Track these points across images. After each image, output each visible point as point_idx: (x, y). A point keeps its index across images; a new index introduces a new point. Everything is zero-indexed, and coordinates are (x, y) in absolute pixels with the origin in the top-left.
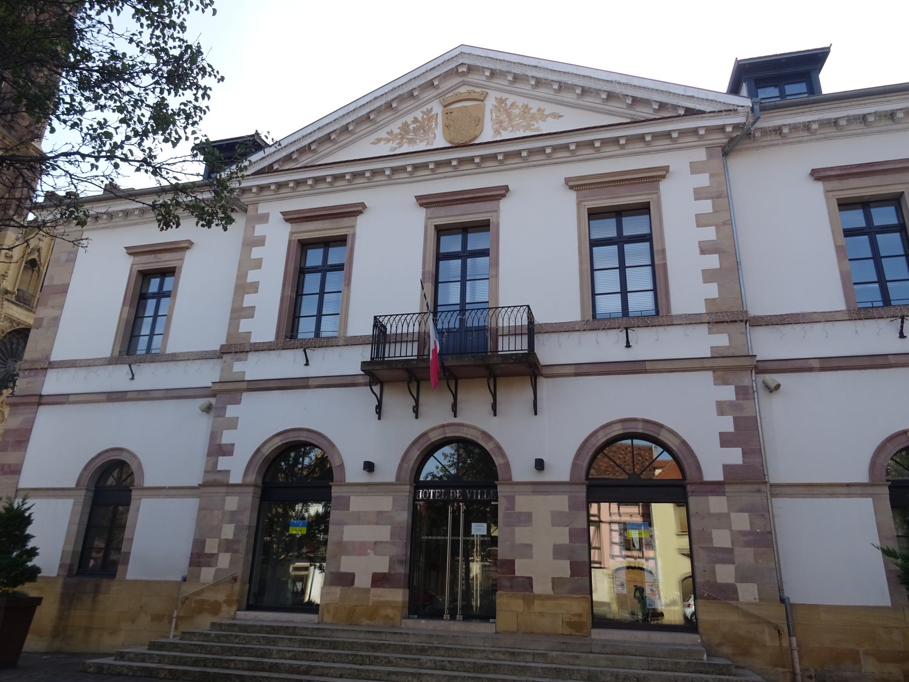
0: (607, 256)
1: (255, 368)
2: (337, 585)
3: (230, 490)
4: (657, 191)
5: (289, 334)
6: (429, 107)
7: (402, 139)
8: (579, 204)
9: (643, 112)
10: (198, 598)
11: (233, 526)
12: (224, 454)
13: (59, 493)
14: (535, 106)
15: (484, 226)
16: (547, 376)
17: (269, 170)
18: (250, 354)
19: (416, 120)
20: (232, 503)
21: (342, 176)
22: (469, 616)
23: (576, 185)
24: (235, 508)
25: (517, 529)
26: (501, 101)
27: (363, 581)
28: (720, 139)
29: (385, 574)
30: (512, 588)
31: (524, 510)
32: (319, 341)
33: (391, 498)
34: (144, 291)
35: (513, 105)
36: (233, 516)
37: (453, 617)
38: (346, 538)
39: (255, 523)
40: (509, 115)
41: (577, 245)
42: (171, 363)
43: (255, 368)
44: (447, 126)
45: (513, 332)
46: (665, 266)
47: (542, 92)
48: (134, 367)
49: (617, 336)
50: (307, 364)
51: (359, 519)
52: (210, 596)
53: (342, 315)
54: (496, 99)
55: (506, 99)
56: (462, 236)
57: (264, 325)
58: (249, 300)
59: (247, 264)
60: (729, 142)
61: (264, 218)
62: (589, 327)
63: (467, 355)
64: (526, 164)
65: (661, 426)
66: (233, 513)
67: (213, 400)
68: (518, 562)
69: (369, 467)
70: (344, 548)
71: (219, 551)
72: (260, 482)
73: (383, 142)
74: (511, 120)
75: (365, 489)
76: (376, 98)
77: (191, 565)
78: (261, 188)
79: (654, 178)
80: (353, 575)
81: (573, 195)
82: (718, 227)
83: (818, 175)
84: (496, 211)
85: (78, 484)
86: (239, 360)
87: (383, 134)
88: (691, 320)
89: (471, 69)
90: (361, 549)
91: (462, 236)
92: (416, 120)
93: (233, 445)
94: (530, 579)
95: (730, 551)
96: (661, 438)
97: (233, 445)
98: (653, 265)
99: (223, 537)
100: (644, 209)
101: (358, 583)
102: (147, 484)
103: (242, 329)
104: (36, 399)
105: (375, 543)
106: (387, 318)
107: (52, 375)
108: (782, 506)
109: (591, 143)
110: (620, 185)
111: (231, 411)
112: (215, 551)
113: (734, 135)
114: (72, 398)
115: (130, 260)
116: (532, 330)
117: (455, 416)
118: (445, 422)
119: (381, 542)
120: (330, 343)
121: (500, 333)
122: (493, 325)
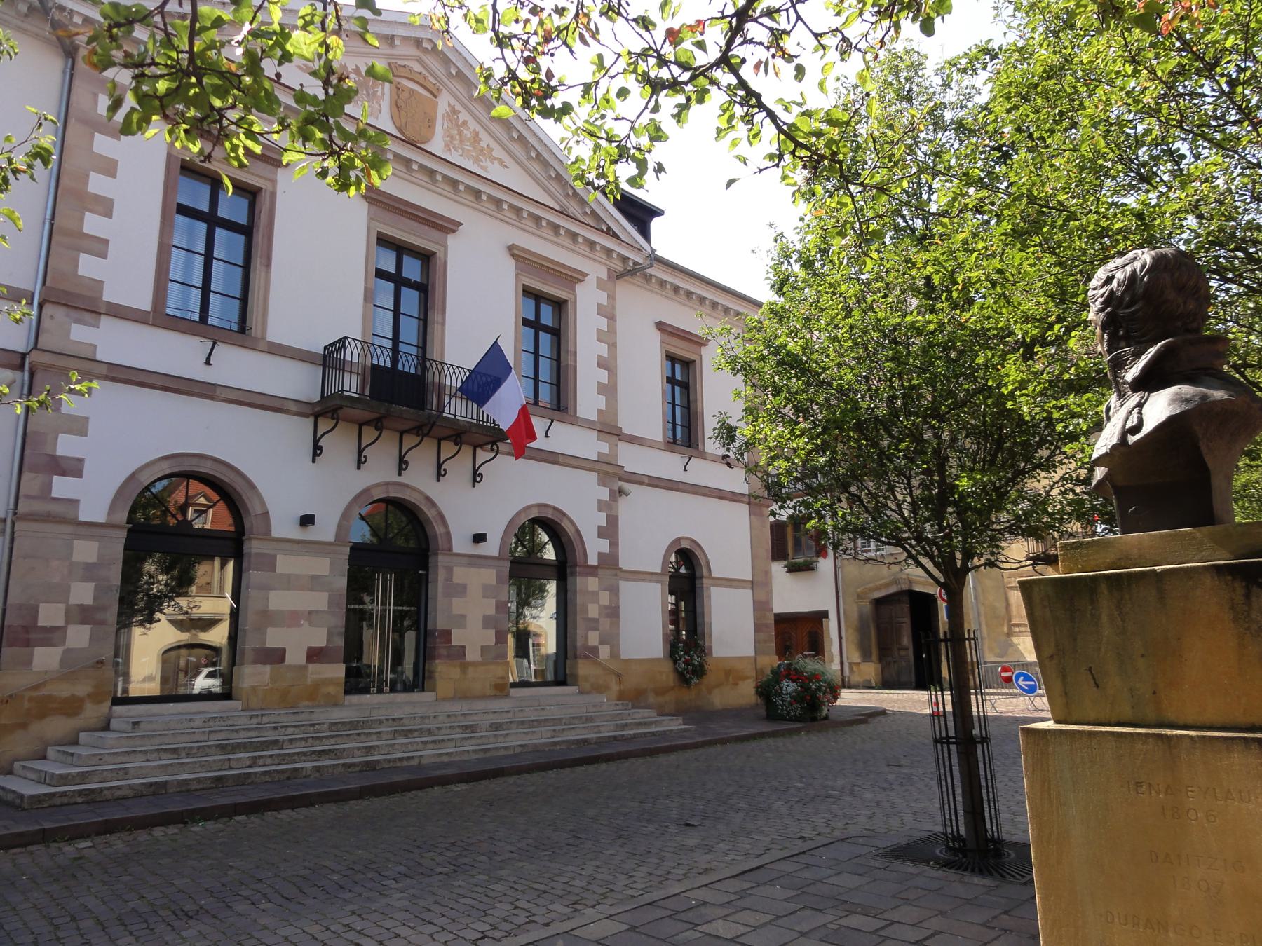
2: (264, 663)
3: (82, 530)
4: (573, 290)
9: (574, 208)
10: (35, 694)
11: (91, 586)
18: (103, 317)
20: (86, 551)
22: (408, 688)
25: (454, 600)
27: (296, 656)
28: (619, 266)
30: (449, 657)
33: (328, 561)
36: (89, 572)
37: (380, 691)
51: (289, 583)
52: (63, 691)
66: (89, 567)
71: (68, 622)
74: (461, 141)
75: (296, 546)
80: (283, 651)
83: (661, 326)
88: (588, 424)
94: (464, 647)
95: (597, 621)
101: (290, 659)
105: (310, 612)
108: (626, 587)
112: (61, 623)
117: (400, 474)
118: (388, 480)
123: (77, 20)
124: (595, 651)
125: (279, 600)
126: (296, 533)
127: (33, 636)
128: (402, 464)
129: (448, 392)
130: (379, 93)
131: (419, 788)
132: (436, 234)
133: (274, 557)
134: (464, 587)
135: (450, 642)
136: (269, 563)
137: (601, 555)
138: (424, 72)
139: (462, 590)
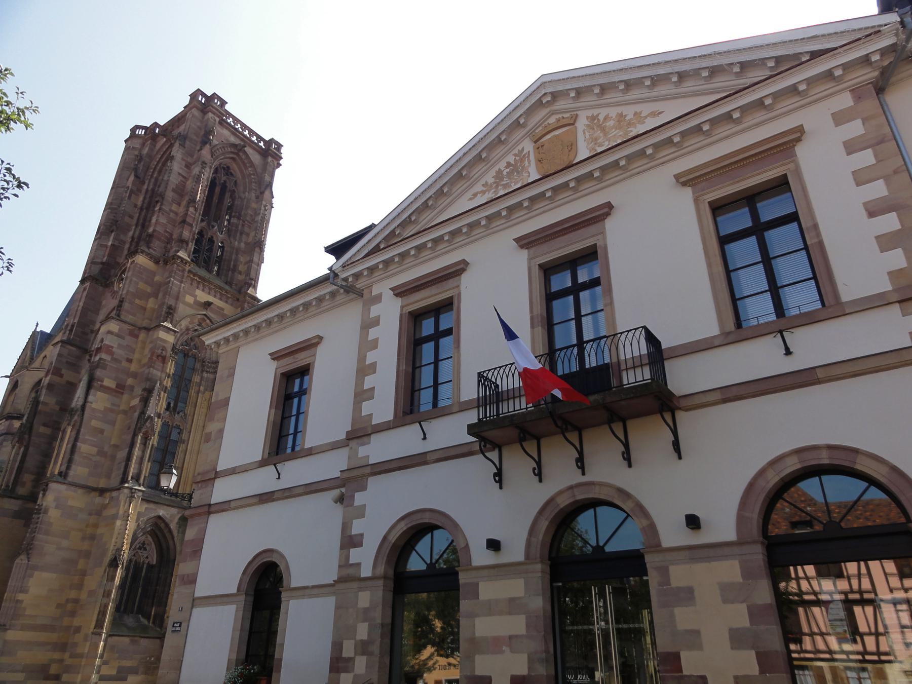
0: (745, 251)
1: (379, 449)
5: (410, 408)
6: (520, 147)
7: (497, 187)
8: (696, 200)
11: (366, 625)
12: (355, 546)
13: (225, 599)
14: (629, 112)
15: (591, 255)
16: (687, 409)
17: (376, 250)
19: (509, 164)
20: (364, 599)
21: (441, 238)
23: (686, 180)
24: (367, 605)
25: (677, 611)
26: (593, 118)
28: (870, 74)
29: (524, 677)
31: (682, 584)
32: (438, 411)
34: (289, 392)
35: (606, 118)
36: (366, 614)
38: (478, 634)
39: (389, 620)
40: (603, 130)
41: (701, 247)
42: (309, 457)
43: (379, 449)
44: (539, 161)
45: (637, 363)
46: (821, 244)
47: (635, 94)
48: (279, 466)
49: (772, 343)
50: (425, 438)
51: (491, 608)
53: (456, 381)
54: (587, 117)
55: (598, 115)
56: (569, 272)
57: (382, 407)
58: (369, 382)
59: (367, 345)
60: (882, 73)
61: (378, 299)
62: (732, 338)
63: (591, 397)
64: (628, 174)
65: (856, 451)
66: (366, 610)
67: (343, 490)
68: (684, 655)
69: (494, 545)
70: (478, 646)
71: (355, 654)
72: (391, 573)
73: (479, 195)
76: (465, 154)
77: (331, 671)
78: (372, 270)
79: (786, 145)
81: (688, 192)
82: (887, 179)
84: (602, 233)
85: (238, 590)
86: (363, 444)
87: (478, 187)
89: (555, 96)
90: (495, 645)
91: (569, 272)
92: (509, 164)
93: (362, 535)
96: (858, 467)
97: (362, 535)
98: (806, 248)
99: (359, 637)
100: (781, 185)
102: (294, 584)
103: (364, 413)
104: (206, 509)
105: (511, 637)
106: (491, 373)
107: (218, 483)
109: (698, 129)
110: (744, 165)
111: (359, 498)
112: (352, 655)
113: (886, 63)
114: (233, 504)
115: (274, 364)
116: (657, 354)
117: (583, 474)
118: (574, 482)
119: (517, 636)
120: (446, 412)
121: (623, 367)
122: (615, 360)
128: (580, 463)
134: (690, 591)
135: (680, 670)
136: (474, 592)
138: (561, 116)
139: (687, 595)
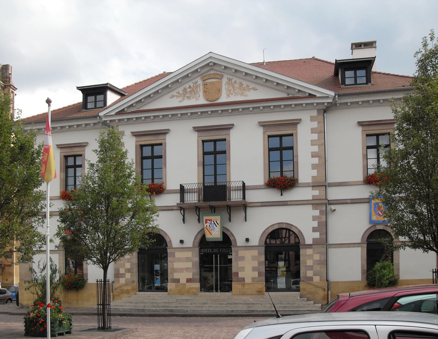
27: (183, 281)
30: (238, 281)
33: (191, 253)
37: (217, 291)
51: (179, 260)
52: (125, 288)
75: (180, 249)
80: (244, 278)
88: (306, 185)
105: (187, 268)
108: (331, 251)
123: (108, 122)
124: (311, 279)
125: (177, 265)
126: (180, 245)
127: (119, 275)
129: (232, 189)
130: (199, 90)
131: (190, 317)
132: (225, 132)
133: (175, 253)
137: (314, 239)
